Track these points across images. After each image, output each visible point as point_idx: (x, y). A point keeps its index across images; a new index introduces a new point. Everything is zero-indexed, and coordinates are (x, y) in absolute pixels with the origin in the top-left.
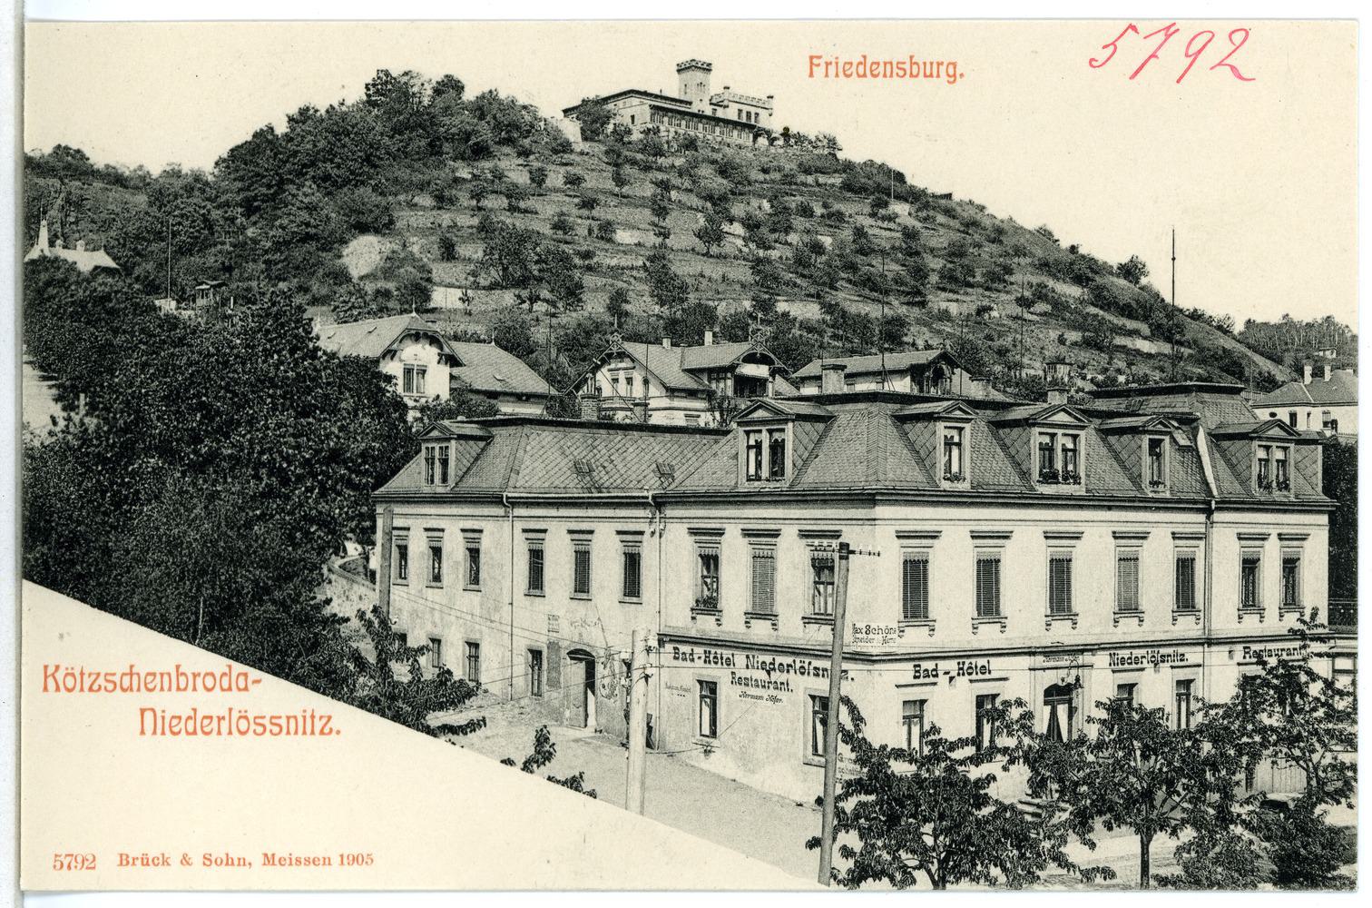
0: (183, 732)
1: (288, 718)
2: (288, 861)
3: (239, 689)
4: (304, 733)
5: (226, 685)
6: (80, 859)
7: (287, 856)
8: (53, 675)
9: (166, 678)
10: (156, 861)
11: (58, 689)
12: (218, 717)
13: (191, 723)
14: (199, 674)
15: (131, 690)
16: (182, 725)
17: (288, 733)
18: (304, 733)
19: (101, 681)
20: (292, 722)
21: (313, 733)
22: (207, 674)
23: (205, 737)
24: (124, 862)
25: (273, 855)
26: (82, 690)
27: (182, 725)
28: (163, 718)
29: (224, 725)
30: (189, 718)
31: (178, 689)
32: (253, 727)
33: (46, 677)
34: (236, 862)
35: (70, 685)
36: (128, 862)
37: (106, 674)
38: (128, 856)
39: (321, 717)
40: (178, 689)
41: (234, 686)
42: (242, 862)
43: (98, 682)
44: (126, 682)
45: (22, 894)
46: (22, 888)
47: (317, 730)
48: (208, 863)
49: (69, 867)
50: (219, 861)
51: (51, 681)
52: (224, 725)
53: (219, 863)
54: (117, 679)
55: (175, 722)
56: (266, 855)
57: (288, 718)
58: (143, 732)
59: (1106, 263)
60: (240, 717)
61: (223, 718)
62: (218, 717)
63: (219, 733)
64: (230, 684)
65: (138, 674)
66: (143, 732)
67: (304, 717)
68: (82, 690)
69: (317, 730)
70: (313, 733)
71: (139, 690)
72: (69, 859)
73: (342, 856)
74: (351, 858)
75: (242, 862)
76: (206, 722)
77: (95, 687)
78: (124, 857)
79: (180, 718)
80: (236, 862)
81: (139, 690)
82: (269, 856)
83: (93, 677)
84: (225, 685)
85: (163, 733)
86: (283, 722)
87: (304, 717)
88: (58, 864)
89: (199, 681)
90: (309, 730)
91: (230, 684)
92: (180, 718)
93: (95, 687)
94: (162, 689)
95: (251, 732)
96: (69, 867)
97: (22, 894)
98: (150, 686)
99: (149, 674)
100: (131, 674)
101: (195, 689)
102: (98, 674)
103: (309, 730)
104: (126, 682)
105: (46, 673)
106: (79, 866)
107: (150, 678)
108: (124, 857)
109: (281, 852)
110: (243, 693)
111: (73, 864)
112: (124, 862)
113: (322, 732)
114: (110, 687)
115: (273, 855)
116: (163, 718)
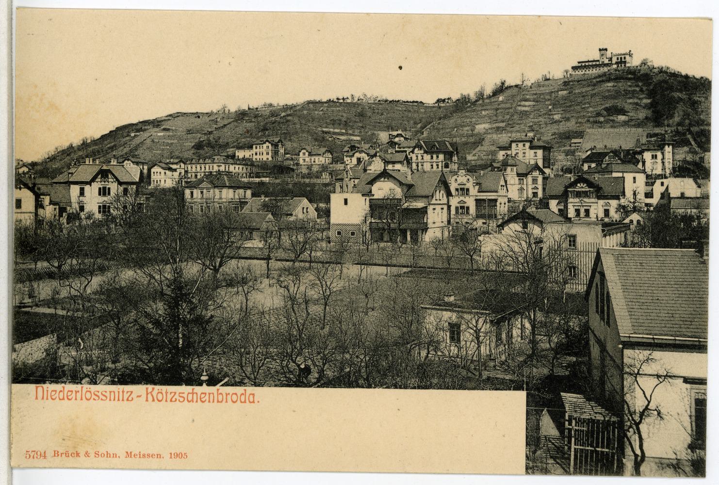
0: (58, 398)
1: (110, 392)
2: (138, 456)
3: (250, 402)
4: (119, 400)
5: (243, 400)
6: (39, 453)
7: (138, 453)
8: (151, 392)
9: (212, 395)
10: (73, 455)
11: (153, 400)
12: (76, 391)
13: (61, 394)
14: (229, 394)
15: (193, 402)
16: (57, 395)
17: (110, 400)
18: (119, 400)
19: (177, 396)
20: (112, 394)
21: (123, 400)
22: (233, 394)
23: (52, 401)
24: (56, 455)
25: (131, 453)
26: (166, 401)
27: (57, 395)
28: (47, 391)
29: (79, 395)
30: (61, 391)
31: (218, 401)
32: (94, 396)
33: (147, 394)
34: (112, 456)
35: (160, 398)
36: (58, 455)
37: (180, 393)
38: (58, 452)
39: (127, 392)
40: (218, 401)
41: (247, 401)
42: (115, 456)
43: (175, 397)
44: (190, 398)
45: (12, 468)
46: (12, 464)
47: (125, 399)
48: (97, 456)
49: (33, 457)
50: (103, 455)
51: (150, 396)
52: (79, 395)
53: (103, 455)
54: (185, 395)
55: (53, 393)
56: (127, 452)
57: (110, 392)
58: (37, 398)
59: (668, 68)
60: (87, 391)
61: (78, 391)
62: (76, 391)
63: (76, 399)
64: (245, 400)
65: (197, 393)
66: (37, 398)
67: (119, 392)
68: (166, 401)
69: (125, 399)
70: (123, 400)
71: (197, 401)
72: (33, 453)
73: (171, 454)
74: (176, 454)
75: (115, 456)
76: (69, 393)
77: (173, 399)
78: (56, 452)
79: (56, 391)
80: (112, 456)
81: (197, 401)
82: (129, 453)
83: (173, 394)
84: (243, 399)
85: (47, 399)
86: (108, 394)
87: (119, 392)
88: (28, 456)
89: (229, 397)
90: (121, 398)
91: (245, 400)
92: (56, 391)
93: (173, 399)
94: (209, 402)
95: (92, 398)
96: (33, 457)
97: (12, 468)
98: (203, 400)
99: (202, 393)
100: (193, 393)
101: (227, 402)
102: (175, 393)
103: (121, 398)
104: (190, 398)
105: (147, 392)
106: (39, 457)
107: (203, 396)
108: (56, 452)
109: (135, 451)
110: (243, 404)
111: (35, 456)
112: (56, 455)
113: (128, 400)
114: (182, 399)
115: (131, 453)
116: (47, 391)
